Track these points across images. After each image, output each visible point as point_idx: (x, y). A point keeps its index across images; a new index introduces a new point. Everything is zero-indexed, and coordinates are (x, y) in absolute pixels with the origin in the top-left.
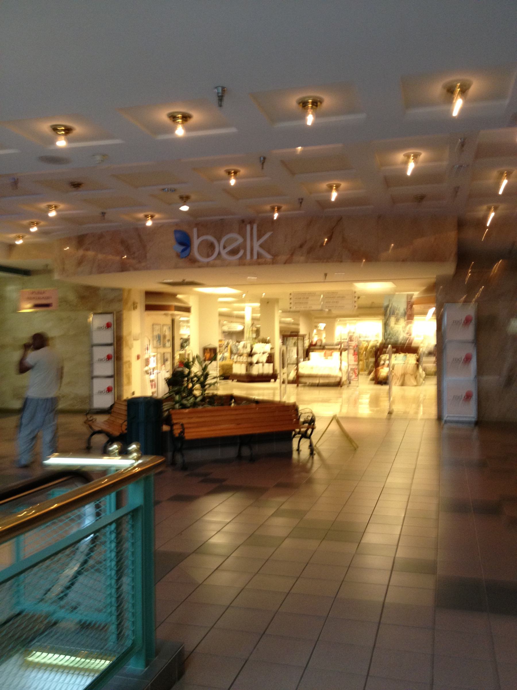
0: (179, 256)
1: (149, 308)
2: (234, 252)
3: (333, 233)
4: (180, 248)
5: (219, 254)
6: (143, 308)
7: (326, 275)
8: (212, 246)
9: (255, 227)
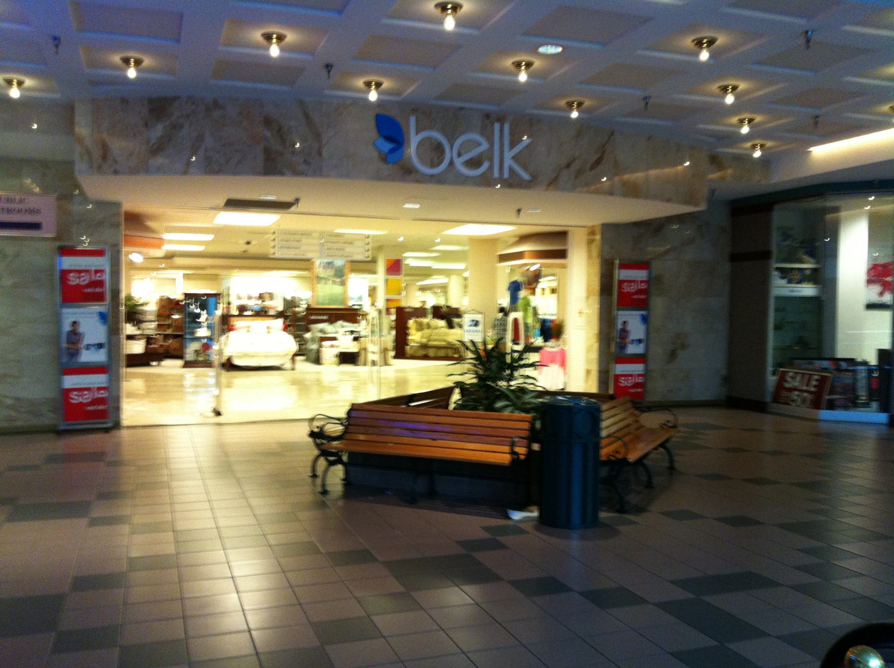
0: (384, 159)
2: (474, 163)
3: (604, 152)
5: (451, 163)
7: (519, 211)
8: (439, 149)
9: (507, 127)
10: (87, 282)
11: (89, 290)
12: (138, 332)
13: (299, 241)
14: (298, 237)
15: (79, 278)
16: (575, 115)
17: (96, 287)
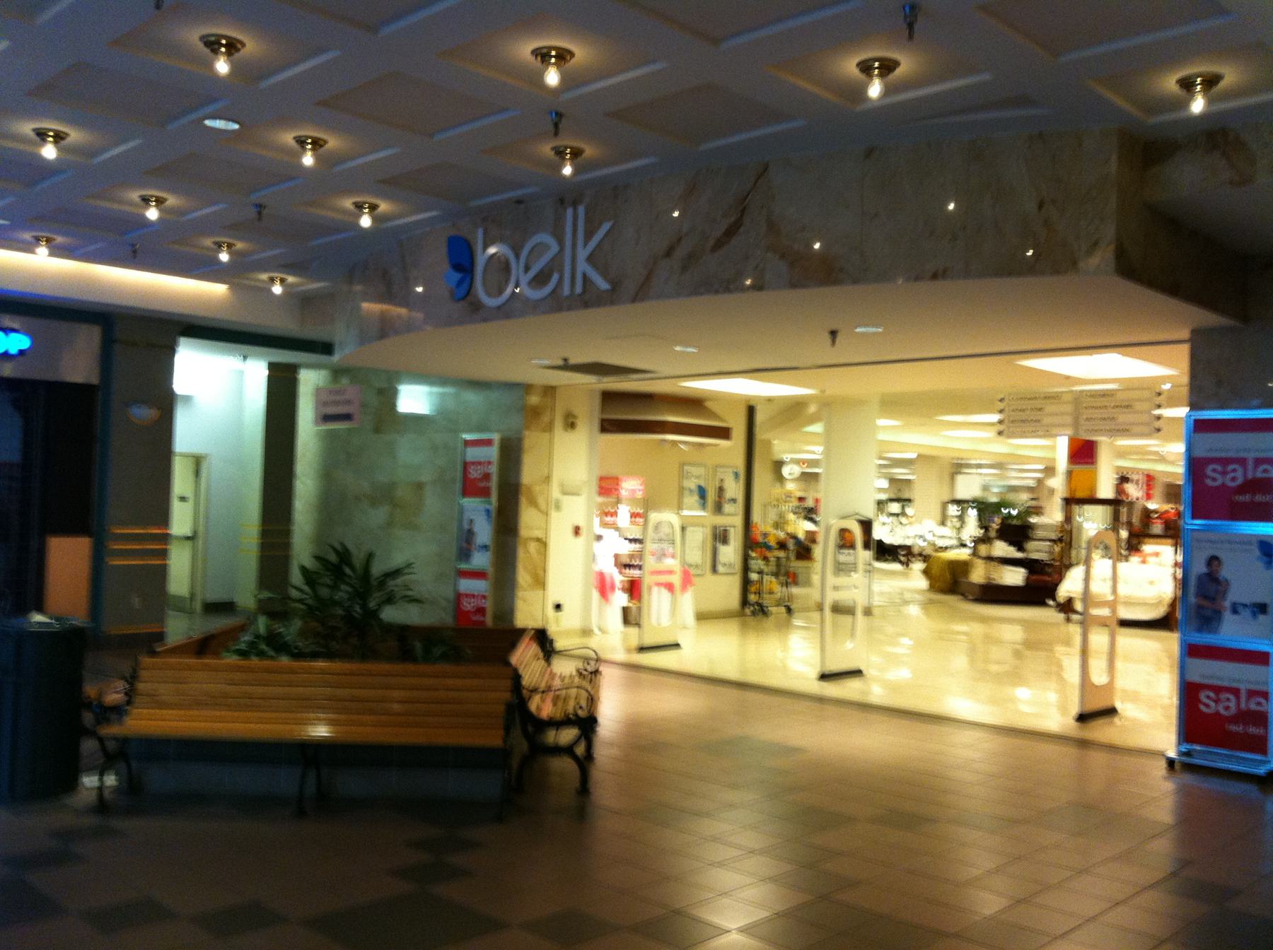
1: (608, 426)
4: (457, 276)
6: (596, 425)
7: (833, 334)
9: (581, 210)
10: (1240, 481)
11: (1246, 498)
12: (1019, 555)
13: (1040, 409)
14: (1038, 404)
15: (1224, 473)
16: (1198, 105)
17: (1254, 494)
